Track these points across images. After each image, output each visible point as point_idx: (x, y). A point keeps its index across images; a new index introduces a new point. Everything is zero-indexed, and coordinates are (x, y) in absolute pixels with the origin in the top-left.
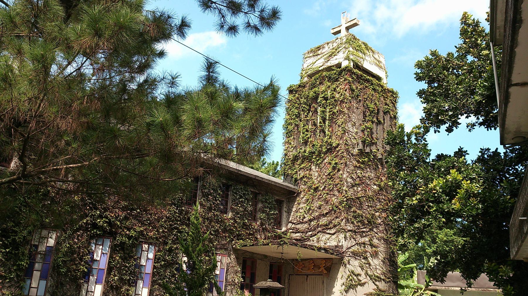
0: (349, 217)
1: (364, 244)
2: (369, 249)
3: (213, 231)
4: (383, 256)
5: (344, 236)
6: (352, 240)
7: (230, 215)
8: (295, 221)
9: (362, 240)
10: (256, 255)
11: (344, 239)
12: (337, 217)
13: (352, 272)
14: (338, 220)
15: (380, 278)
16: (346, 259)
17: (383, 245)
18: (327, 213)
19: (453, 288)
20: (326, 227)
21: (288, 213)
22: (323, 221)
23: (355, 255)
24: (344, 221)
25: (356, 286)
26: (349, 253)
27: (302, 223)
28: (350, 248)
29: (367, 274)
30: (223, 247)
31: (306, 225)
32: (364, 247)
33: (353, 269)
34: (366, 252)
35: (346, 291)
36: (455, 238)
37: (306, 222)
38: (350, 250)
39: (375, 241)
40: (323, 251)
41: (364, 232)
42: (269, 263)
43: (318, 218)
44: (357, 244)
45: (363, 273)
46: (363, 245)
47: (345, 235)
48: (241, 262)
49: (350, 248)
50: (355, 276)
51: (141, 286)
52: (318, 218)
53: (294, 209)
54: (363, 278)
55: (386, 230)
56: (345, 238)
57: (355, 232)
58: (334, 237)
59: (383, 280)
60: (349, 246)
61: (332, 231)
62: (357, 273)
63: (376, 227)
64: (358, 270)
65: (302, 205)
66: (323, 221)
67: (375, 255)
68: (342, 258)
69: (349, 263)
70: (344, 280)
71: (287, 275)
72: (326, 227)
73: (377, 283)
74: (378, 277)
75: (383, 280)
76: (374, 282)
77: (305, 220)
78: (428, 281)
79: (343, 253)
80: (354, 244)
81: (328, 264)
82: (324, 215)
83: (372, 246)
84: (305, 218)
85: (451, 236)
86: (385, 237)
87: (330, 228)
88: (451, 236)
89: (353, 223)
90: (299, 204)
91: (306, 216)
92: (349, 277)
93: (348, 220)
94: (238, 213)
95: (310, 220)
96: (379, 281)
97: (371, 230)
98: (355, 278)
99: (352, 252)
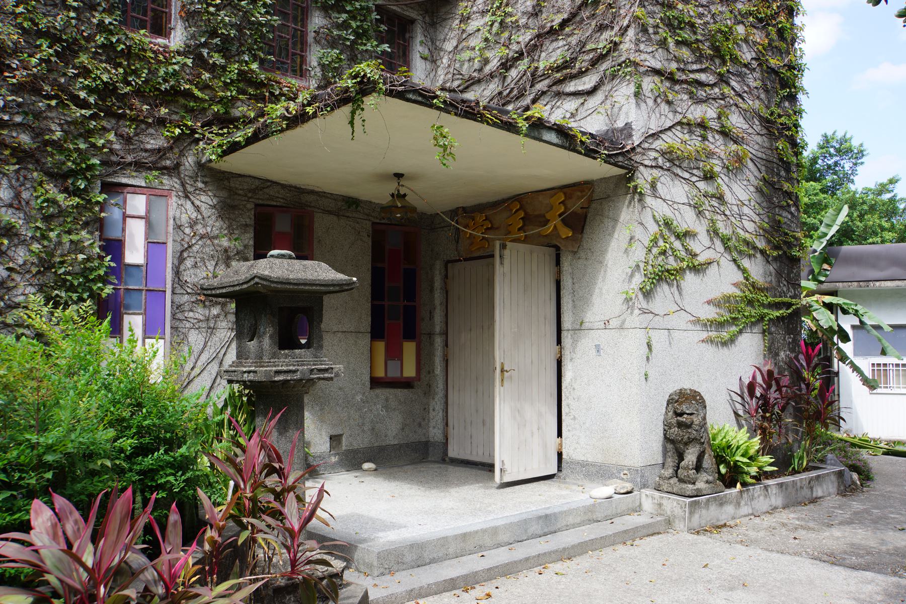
0: (651, 21)
1: (702, 125)
2: (717, 144)
3: (90, 91)
4: (757, 173)
5: (632, 89)
6: (664, 107)
7: (177, 38)
8: (456, 83)
9: (696, 113)
10: (311, 198)
11: (633, 100)
12: (601, 28)
13: (668, 224)
14: (607, 35)
15: (755, 248)
16: (644, 177)
17: (759, 139)
18: (564, 24)
19: (878, 284)
20: (566, 70)
21: (434, 61)
22: (554, 53)
23: (673, 161)
24: (631, 32)
25: (681, 271)
26: (653, 154)
27: (479, 81)
28: (655, 136)
29: (714, 232)
30: (159, 164)
31: (493, 87)
32: (704, 138)
33: (668, 213)
34: (710, 155)
35: (648, 294)
36: (825, 198)
37: (492, 76)
38: (658, 144)
39: (736, 121)
40: (552, 137)
41: (700, 84)
42: (368, 225)
43: (533, 48)
44: (680, 123)
45: (701, 228)
46: (698, 131)
47: (639, 87)
48: (248, 218)
49: (655, 136)
50: (678, 237)
51: (139, 332)
52: (533, 48)
53: (449, 46)
54: (702, 247)
55: (767, 91)
56: (638, 94)
57: (671, 78)
58: (594, 101)
59: (763, 252)
60: (654, 128)
61: (587, 82)
62: (683, 228)
63: (740, 75)
64: (687, 220)
65: (474, 25)
66: (554, 53)
67: (735, 166)
68: (630, 172)
69: (653, 186)
70: (639, 254)
71: (439, 265)
72: (566, 70)
73: (746, 263)
74: (747, 243)
75: (763, 252)
76: (734, 261)
77: (488, 69)
78: (816, 271)
79: (633, 149)
80: (669, 124)
81: (576, 206)
82: (553, 33)
83: (725, 133)
84: (486, 61)
85: (816, 194)
86: (765, 113)
87: (581, 74)
88: (816, 194)
89: (663, 43)
90: (465, 19)
91: (489, 54)
92: (655, 241)
93: (644, 30)
94: (213, 34)
95: (506, 65)
96: (750, 256)
97: (723, 79)
98: (677, 244)
99: (663, 154)
